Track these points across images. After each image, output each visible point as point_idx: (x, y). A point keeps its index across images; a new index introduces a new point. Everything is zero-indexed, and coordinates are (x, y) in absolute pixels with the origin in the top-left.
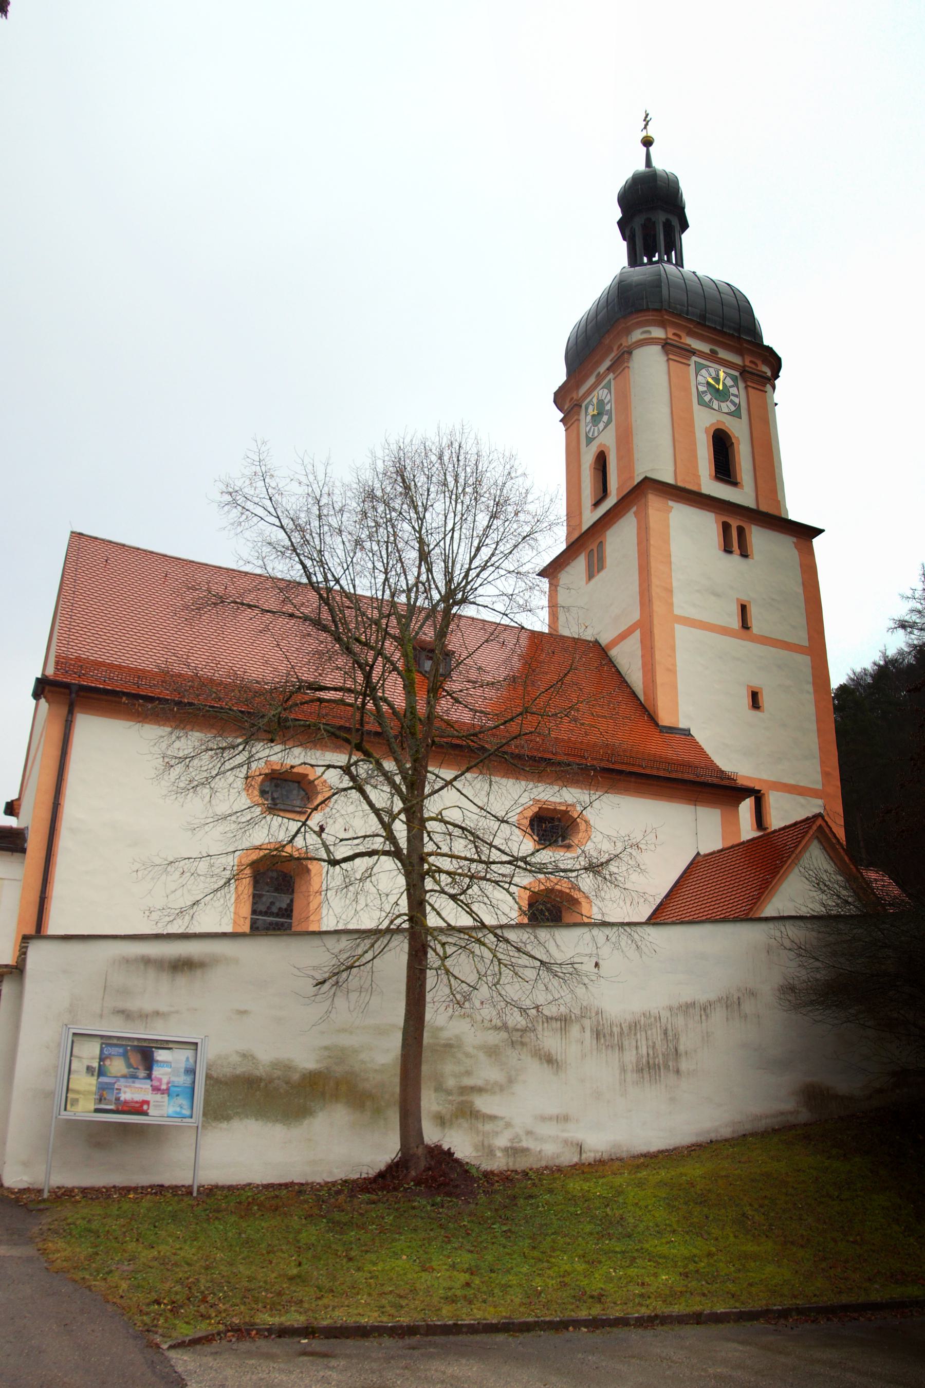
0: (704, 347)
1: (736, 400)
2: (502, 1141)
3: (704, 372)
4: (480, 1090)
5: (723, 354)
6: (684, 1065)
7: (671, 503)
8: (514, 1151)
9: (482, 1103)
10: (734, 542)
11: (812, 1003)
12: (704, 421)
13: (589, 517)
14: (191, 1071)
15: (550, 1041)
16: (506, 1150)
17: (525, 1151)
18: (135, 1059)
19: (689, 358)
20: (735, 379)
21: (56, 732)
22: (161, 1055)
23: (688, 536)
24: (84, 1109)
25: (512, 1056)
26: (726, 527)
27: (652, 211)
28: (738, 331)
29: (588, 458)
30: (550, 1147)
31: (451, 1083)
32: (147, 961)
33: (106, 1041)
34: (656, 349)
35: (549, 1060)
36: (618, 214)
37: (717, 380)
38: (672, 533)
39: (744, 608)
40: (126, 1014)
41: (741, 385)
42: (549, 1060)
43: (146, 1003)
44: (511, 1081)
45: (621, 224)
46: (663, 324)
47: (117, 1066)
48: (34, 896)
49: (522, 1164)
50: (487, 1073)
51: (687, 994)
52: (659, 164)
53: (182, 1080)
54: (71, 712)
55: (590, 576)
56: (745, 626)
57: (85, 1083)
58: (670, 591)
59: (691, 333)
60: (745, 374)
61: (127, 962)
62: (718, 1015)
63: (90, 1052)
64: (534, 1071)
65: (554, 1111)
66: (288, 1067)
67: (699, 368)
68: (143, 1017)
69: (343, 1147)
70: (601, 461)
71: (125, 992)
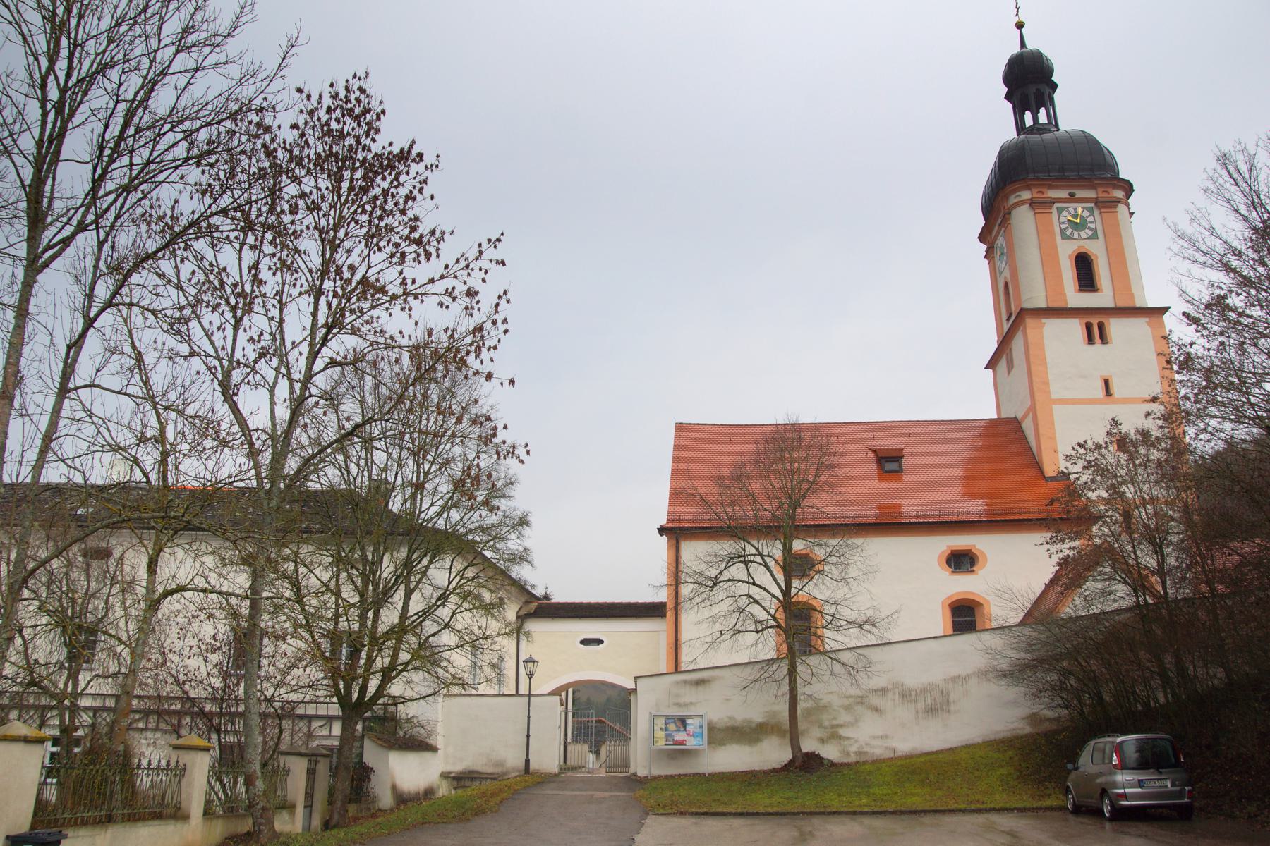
0: (1063, 194)
1: (1093, 226)
2: (854, 749)
3: (1064, 213)
4: (838, 726)
5: (1080, 193)
6: (952, 708)
7: (1044, 321)
8: (859, 753)
9: (842, 732)
10: (1096, 334)
11: (1005, 675)
12: (1066, 252)
13: (1006, 327)
14: (701, 727)
15: (876, 701)
17: (866, 753)
18: (679, 723)
19: (1050, 207)
20: (1090, 210)
22: (689, 721)
23: (1060, 341)
24: (661, 743)
25: (859, 709)
26: (1089, 328)
27: (1029, 80)
28: (1092, 170)
29: (1001, 286)
30: (878, 750)
31: (827, 723)
32: (685, 682)
33: (667, 717)
34: (1027, 206)
35: (877, 710)
36: (1004, 90)
37: (1075, 216)
38: (1046, 342)
39: (1106, 382)
40: (678, 705)
41: (1096, 212)
42: (877, 710)
43: (687, 699)
44: (857, 721)
45: (1008, 97)
46: (1028, 188)
47: (672, 727)
48: (673, 640)
49: (863, 759)
50: (845, 717)
51: (954, 672)
52: (1031, 45)
53: (698, 730)
54: (678, 542)
55: (1009, 373)
56: (1108, 392)
57: (660, 734)
58: (1047, 383)
59: (1051, 187)
60: (1097, 202)
61: (677, 683)
62: (973, 681)
63: (660, 722)
64: (869, 716)
65: (880, 733)
66: (750, 721)
67: (1060, 211)
68: (686, 705)
69: (774, 754)
70: (1006, 285)
71: (677, 696)
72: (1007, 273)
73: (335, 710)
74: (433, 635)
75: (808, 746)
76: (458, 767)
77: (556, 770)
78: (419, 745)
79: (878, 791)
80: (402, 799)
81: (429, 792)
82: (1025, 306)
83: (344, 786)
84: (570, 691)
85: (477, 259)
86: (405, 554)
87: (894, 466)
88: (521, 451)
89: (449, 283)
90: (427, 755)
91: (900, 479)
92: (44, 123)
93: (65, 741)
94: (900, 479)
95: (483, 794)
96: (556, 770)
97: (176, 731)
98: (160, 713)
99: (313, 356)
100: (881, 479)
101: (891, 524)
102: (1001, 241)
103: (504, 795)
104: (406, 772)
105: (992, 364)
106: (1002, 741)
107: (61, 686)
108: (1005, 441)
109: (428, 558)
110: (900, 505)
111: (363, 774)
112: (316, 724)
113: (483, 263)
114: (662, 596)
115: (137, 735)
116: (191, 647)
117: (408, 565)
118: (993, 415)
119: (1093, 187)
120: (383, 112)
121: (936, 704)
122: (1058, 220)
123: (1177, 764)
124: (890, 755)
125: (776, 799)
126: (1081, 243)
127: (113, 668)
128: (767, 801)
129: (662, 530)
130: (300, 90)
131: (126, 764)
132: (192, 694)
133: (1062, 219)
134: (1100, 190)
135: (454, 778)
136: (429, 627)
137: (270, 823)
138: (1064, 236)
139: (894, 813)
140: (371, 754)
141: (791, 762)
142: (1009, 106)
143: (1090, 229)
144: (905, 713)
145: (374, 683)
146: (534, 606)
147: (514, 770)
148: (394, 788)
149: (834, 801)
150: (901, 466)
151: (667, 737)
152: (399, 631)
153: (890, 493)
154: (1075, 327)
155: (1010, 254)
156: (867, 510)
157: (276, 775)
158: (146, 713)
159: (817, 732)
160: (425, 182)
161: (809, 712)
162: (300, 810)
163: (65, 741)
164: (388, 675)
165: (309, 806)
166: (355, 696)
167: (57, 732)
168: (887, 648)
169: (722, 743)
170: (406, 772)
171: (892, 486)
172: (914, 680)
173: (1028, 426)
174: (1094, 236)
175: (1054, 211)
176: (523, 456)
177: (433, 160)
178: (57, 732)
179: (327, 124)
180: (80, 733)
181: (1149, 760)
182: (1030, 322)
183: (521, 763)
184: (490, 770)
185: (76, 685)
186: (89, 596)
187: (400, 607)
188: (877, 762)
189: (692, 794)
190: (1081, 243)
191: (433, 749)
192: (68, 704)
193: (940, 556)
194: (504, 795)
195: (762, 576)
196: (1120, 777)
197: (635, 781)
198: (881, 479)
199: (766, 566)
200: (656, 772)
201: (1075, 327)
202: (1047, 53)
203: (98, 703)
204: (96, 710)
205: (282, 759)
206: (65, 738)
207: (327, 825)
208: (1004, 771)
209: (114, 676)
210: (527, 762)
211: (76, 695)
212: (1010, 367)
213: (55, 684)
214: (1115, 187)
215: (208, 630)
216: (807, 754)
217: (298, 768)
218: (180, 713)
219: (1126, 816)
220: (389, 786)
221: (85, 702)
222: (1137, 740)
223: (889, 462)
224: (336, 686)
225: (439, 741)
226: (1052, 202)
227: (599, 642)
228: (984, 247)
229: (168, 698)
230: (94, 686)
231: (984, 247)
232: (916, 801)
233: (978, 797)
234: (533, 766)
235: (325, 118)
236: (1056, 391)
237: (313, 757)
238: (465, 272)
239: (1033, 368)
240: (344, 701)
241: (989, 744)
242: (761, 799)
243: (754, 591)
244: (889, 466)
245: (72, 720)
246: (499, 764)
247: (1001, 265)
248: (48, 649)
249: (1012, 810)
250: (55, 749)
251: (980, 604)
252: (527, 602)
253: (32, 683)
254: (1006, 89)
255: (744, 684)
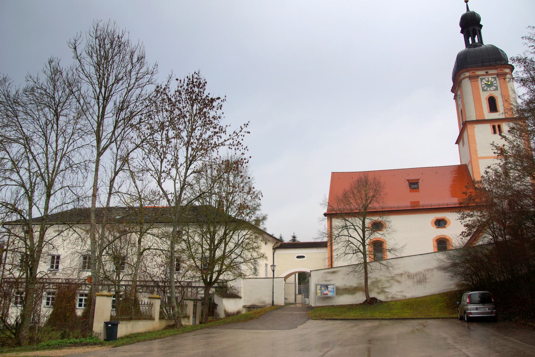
0: (483, 72)
1: (496, 85)
2: (390, 296)
3: (484, 80)
5: (490, 72)
6: (427, 281)
9: (386, 290)
12: (484, 96)
15: (399, 278)
16: (391, 298)
19: (478, 79)
20: (495, 78)
21: (329, 222)
22: (329, 287)
25: (392, 281)
26: (494, 127)
27: (470, 24)
28: (495, 61)
30: (399, 296)
31: (380, 287)
32: (328, 272)
33: (321, 285)
34: (467, 79)
35: (399, 282)
36: (460, 29)
38: (476, 134)
41: (497, 79)
42: (399, 282)
43: (328, 279)
44: (391, 286)
45: (462, 32)
46: (468, 71)
47: (323, 289)
49: (394, 299)
50: (387, 285)
51: (428, 267)
52: (471, 10)
53: (332, 290)
54: (331, 219)
57: (319, 291)
58: (476, 151)
59: (477, 70)
60: (498, 75)
62: (435, 271)
63: (319, 287)
64: (396, 284)
66: (352, 286)
67: (482, 80)
68: (329, 281)
69: (360, 298)
71: (326, 277)
72: (461, 106)
73: (202, 284)
74: (236, 258)
75: (372, 295)
76: (249, 304)
77: (283, 304)
78: (235, 296)
79: (394, 311)
80: (228, 315)
81: (238, 313)
82: (468, 120)
83: (206, 310)
84: (297, 274)
85: (241, 131)
86: (223, 231)
87: (415, 186)
88: (260, 196)
89: (231, 141)
90: (238, 300)
91: (419, 191)
92: (99, 111)
93: (117, 296)
94: (419, 191)
95: (255, 313)
96: (283, 304)
97: (152, 292)
98: (148, 287)
99: (187, 169)
100: (410, 191)
101: (415, 209)
102: (459, 93)
103: (262, 313)
104: (229, 306)
105: (457, 142)
106: (444, 293)
107: (115, 278)
108: (462, 172)
109: (232, 232)
110: (419, 202)
111: (215, 306)
112: (199, 289)
113: (243, 133)
114: (325, 239)
115: (139, 294)
116: (155, 267)
117: (225, 234)
118: (459, 163)
119: (496, 69)
120: (206, 82)
121: (421, 279)
122: (481, 84)
123: (491, 302)
124: (403, 298)
125: (357, 314)
126: (491, 92)
127: (130, 272)
128: (353, 315)
129: (325, 215)
130: (177, 80)
131: (136, 302)
132: (156, 280)
133: (483, 83)
134: (499, 69)
135: (248, 308)
136: (233, 256)
137: (180, 321)
138: (484, 90)
139: (397, 319)
140: (217, 299)
141: (366, 301)
142: (462, 35)
143: (495, 86)
144: (409, 283)
145: (215, 276)
146: (279, 244)
147: (269, 304)
148: (225, 311)
149: (377, 315)
150: (418, 186)
151: (321, 292)
152: (224, 257)
153: (415, 197)
154: (488, 128)
155: (462, 98)
156: (406, 204)
157: (182, 306)
158: (142, 286)
159: (376, 290)
160: (221, 106)
161: (373, 283)
162: (191, 318)
163: (117, 296)
164: (220, 272)
165: (195, 317)
166: (208, 280)
167: (114, 293)
168: (399, 259)
169: (342, 294)
170: (229, 306)
171: (415, 194)
172: (413, 270)
173: (469, 167)
174: (496, 89)
175: (479, 80)
176: (261, 197)
177: (224, 98)
178: (114, 293)
179: (187, 89)
180: (121, 293)
181: (483, 300)
182: (469, 127)
183: (271, 302)
184: (260, 305)
185: (119, 278)
186: (121, 248)
187: (223, 249)
188: (397, 301)
189: (328, 313)
190: (491, 92)
191: (240, 298)
192: (117, 283)
193: (432, 221)
194: (262, 313)
195: (355, 234)
196: (470, 306)
197: (310, 308)
198: (410, 191)
199: (355, 229)
200: (318, 304)
201: (488, 128)
202: (477, 11)
203: (127, 283)
204: (126, 286)
205: (185, 301)
206: (117, 295)
207: (201, 323)
208: (441, 304)
209: (131, 274)
210: (273, 301)
211: (119, 281)
212: (463, 144)
213: (113, 278)
214: (505, 68)
215: (159, 260)
216: (372, 298)
217: (190, 304)
218: (153, 286)
219: (472, 320)
220: (223, 310)
221: (122, 283)
222: (483, 294)
223: (414, 185)
224: (202, 276)
225: (242, 295)
226: (478, 76)
227: (304, 257)
228: (454, 94)
229: (148, 281)
230: (125, 277)
231: (454, 94)
232: (406, 315)
233: (430, 314)
234: (275, 303)
235: (186, 88)
236: (480, 154)
237: (195, 301)
238: (236, 137)
239: (470, 144)
240: (205, 281)
241: (439, 294)
242: (352, 315)
243: (351, 239)
244: (413, 186)
245: (119, 289)
246: (263, 302)
247: (460, 102)
248: (110, 266)
249: (439, 318)
250: (114, 299)
251: (448, 240)
252: (277, 243)
253: (106, 277)
254: (460, 29)
255: (348, 273)
